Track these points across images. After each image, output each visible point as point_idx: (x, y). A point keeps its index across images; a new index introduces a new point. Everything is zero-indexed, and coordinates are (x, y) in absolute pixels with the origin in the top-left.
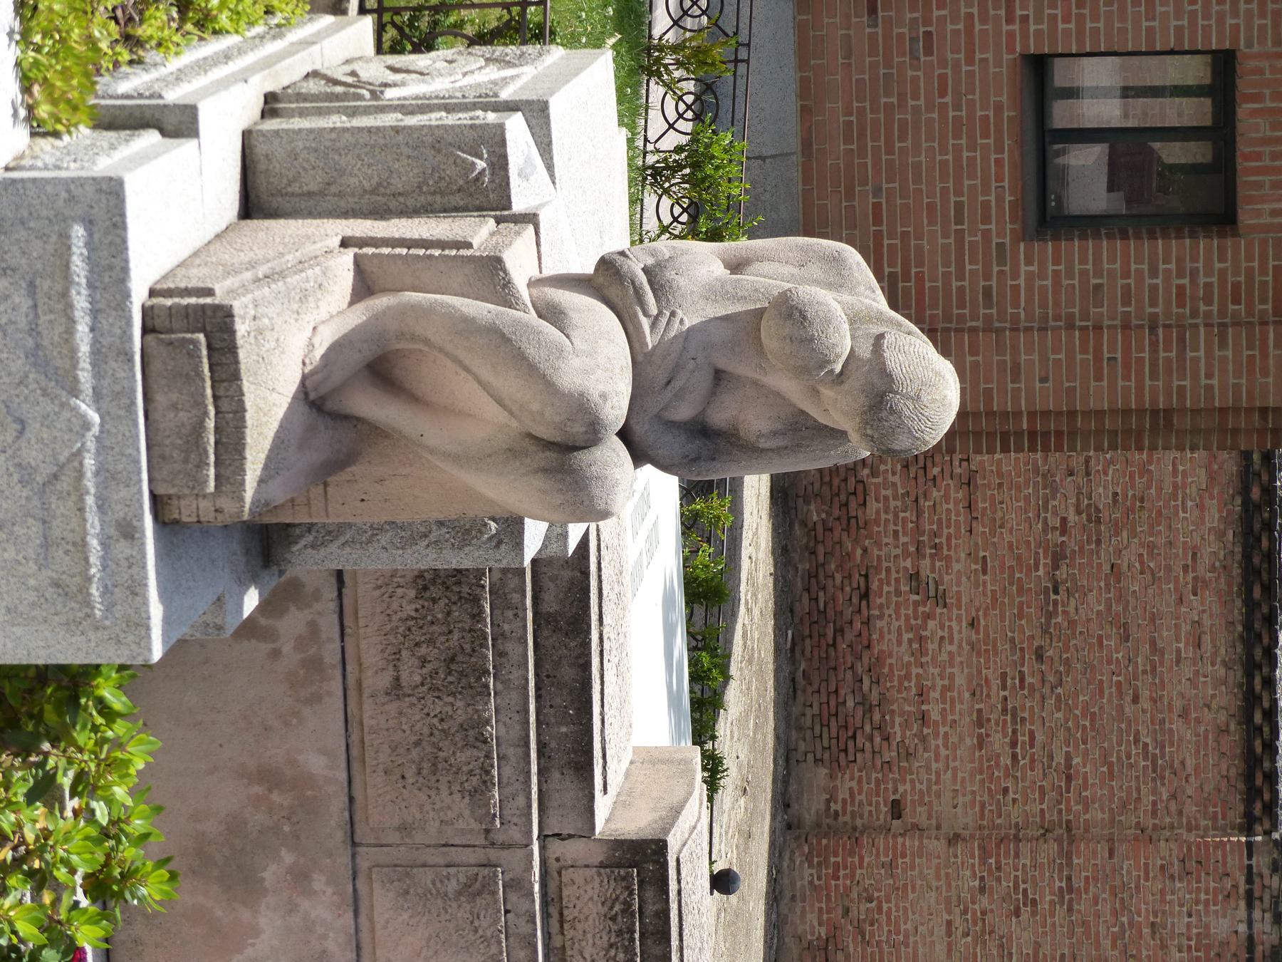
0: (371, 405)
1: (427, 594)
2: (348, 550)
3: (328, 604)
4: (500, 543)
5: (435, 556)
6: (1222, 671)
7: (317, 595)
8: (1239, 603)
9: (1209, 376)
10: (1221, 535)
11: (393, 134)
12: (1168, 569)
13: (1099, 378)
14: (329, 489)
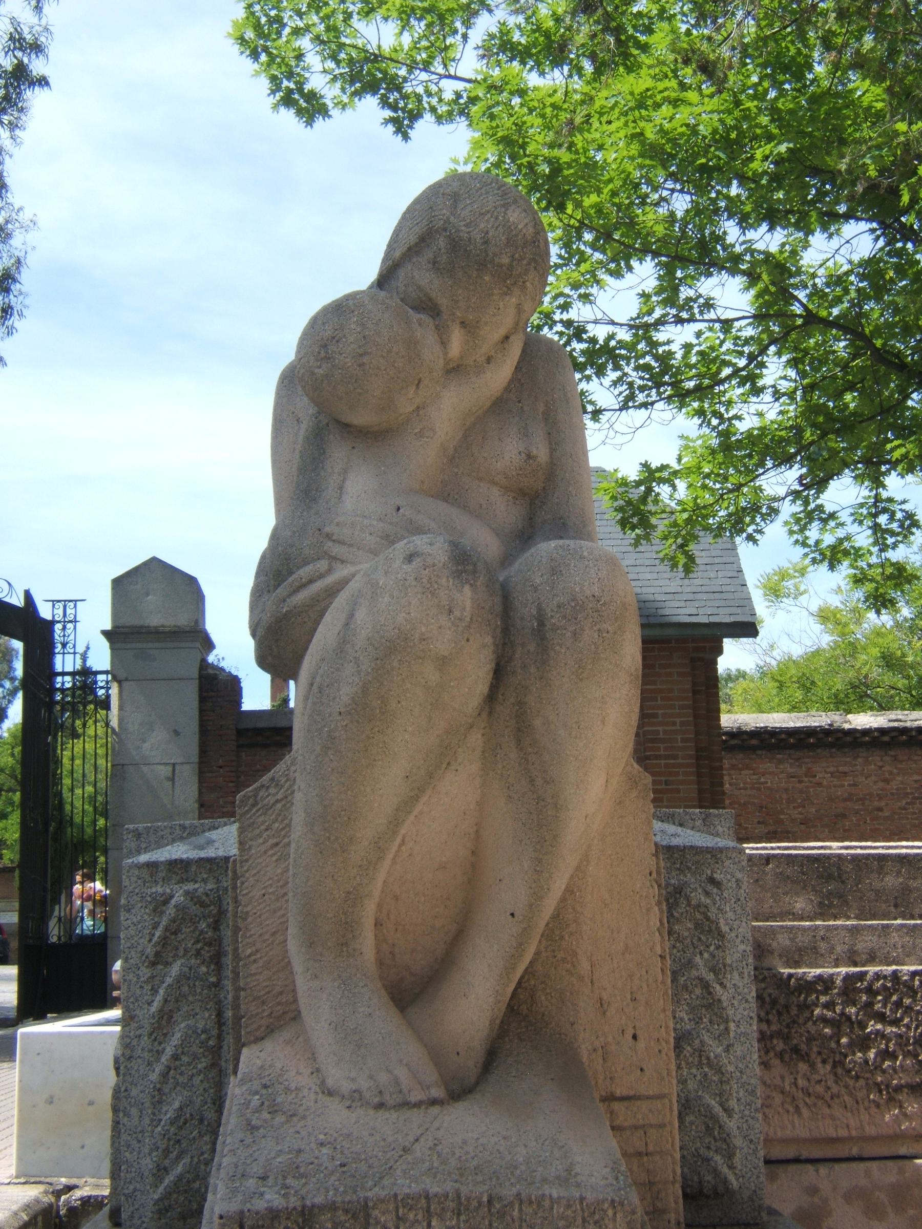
0: (473, 1003)
1: (803, 1047)
2: (733, 1103)
3: (821, 1176)
4: (712, 881)
5: (735, 974)
6: (860, 760)
7: (813, 1191)
8: (819, 751)
9: (674, 724)
10: (780, 762)
11: (134, 1025)
12: (801, 792)
13: (678, 791)
14: (618, 1093)
